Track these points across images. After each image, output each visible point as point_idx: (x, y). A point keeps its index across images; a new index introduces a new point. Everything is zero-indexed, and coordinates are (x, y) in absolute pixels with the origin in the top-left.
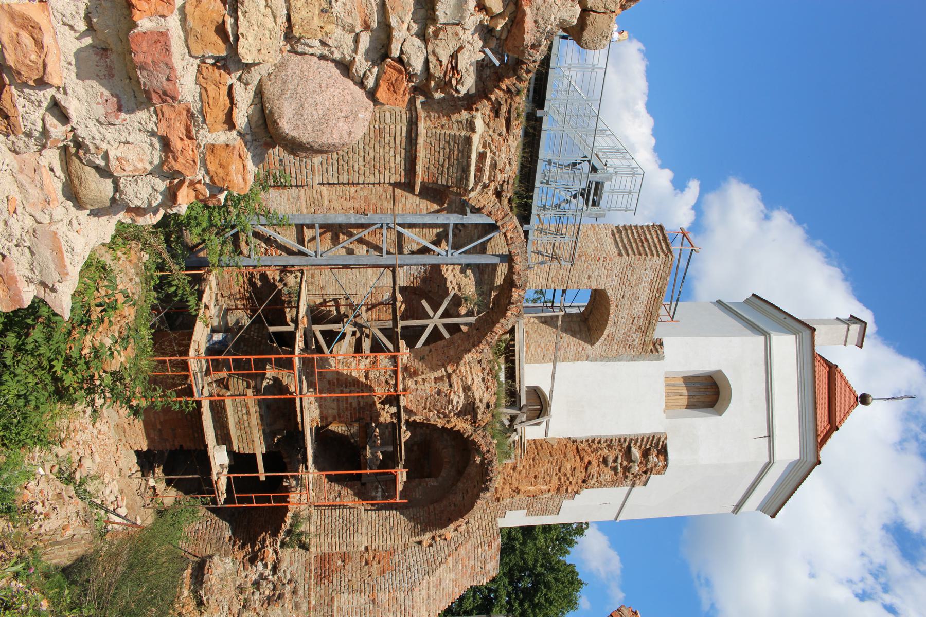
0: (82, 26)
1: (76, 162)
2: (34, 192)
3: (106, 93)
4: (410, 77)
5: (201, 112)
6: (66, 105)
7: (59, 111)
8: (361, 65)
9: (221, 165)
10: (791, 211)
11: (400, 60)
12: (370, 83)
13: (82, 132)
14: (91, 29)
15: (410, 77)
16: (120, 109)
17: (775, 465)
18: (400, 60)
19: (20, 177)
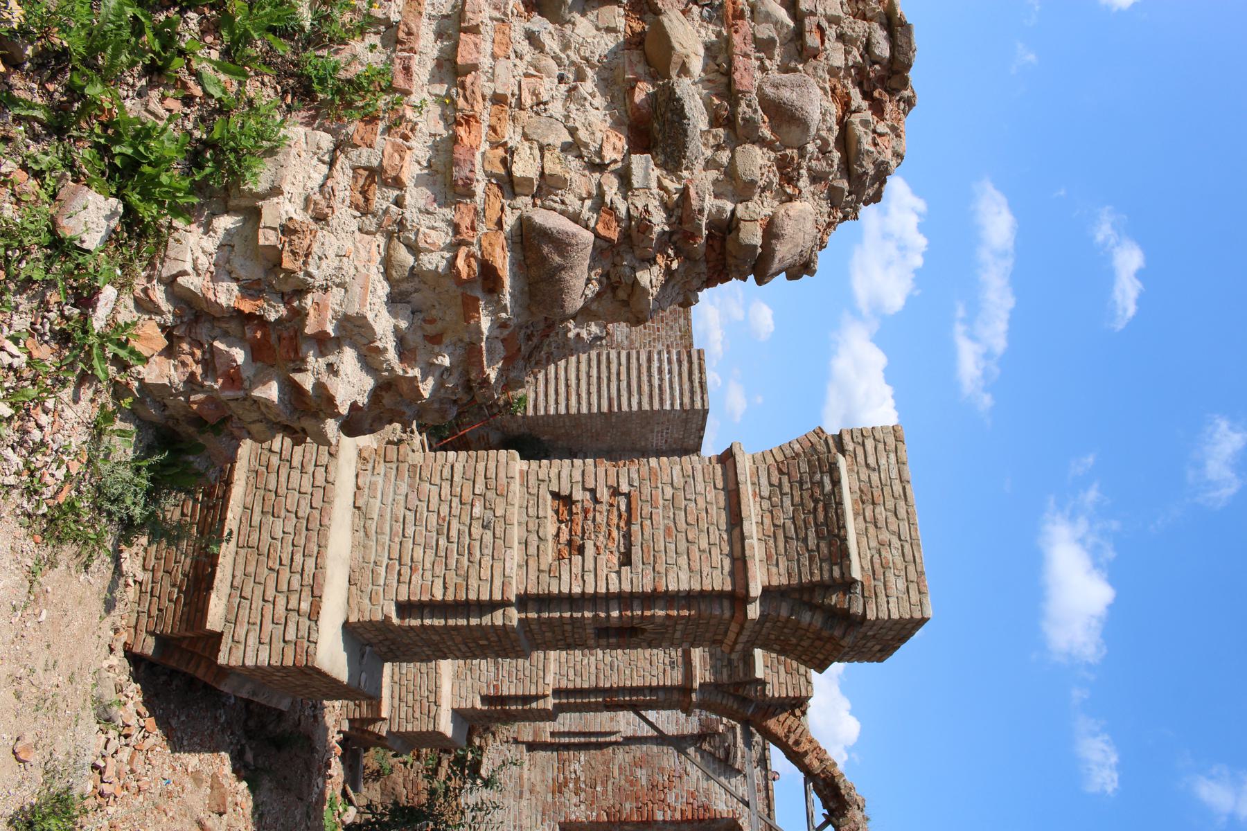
0: (425, 164)
1: (396, 240)
2: (363, 254)
3: (429, 193)
4: (618, 220)
5: (484, 210)
6: (363, 374)
7: (399, 202)
8: (586, 213)
9: (490, 244)
10: (1117, 599)
11: (611, 208)
12: (592, 223)
13: (407, 215)
14: (429, 166)
15: (618, 220)
16: (435, 201)
17: (917, 39)
18: (611, 208)
19: (359, 245)
